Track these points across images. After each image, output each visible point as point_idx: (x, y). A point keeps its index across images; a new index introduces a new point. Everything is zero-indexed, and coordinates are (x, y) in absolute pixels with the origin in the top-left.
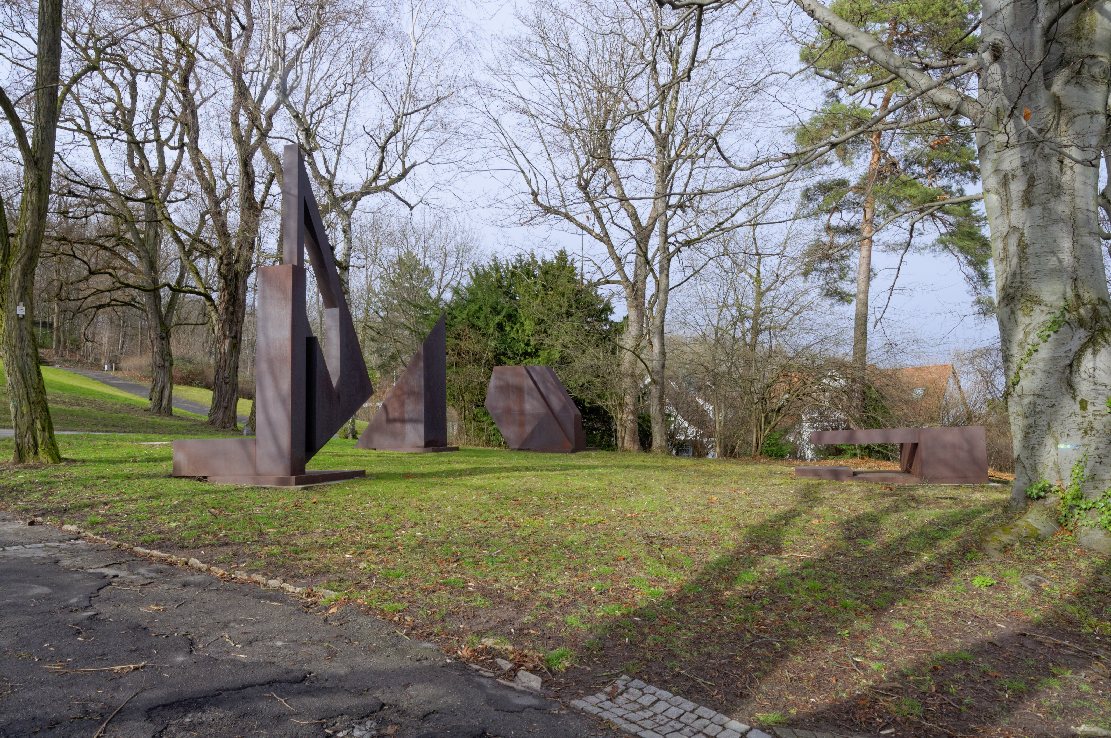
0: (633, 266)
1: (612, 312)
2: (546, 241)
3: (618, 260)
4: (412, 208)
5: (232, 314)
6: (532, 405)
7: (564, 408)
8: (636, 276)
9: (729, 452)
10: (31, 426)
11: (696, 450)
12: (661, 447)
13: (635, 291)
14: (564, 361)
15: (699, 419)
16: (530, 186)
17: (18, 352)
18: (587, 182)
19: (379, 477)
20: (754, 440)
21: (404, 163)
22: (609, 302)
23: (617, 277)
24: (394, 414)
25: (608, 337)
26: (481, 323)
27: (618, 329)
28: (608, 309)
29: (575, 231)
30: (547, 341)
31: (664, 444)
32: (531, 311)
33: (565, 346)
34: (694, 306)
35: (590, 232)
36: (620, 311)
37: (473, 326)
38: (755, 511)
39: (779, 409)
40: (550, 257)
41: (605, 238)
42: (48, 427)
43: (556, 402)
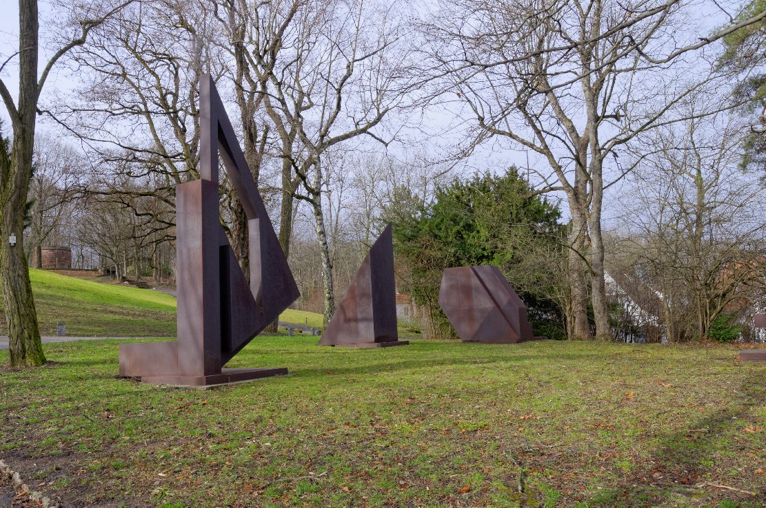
0: (573, 175)
1: (559, 215)
2: (494, 159)
3: (558, 169)
4: (387, 145)
5: (243, 239)
6: (483, 303)
7: (510, 303)
8: (577, 182)
9: (681, 337)
10: (20, 336)
11: (648, 335)
12: (603, 335)
13: (576, 195)
14: (516, 260)
15: (652, 306)
16: (477, 114)
17: (11, 273)
18: (525, 103)
19: (297, 374)
20: (701, 324)
21: (378, 110)
22: (557, 207)
23: (559, 184)
24: (350, 315)
25: (555, 237)
26: (442, 234)
27: (564, 230)
28: (556, 213)
29: (521, 149)
30: (500, 245)
31: (607, 331)
32: (483, 220)
33: (515, 248)
34: (630, 207)
35: (532, 146)
36: (566, 215)
37: (436, 236)
38: (676, 411)
39: (724, 295)
40: (501, 174)
41: (546, 151)
42: (36, 336)
43: (503, 298)
